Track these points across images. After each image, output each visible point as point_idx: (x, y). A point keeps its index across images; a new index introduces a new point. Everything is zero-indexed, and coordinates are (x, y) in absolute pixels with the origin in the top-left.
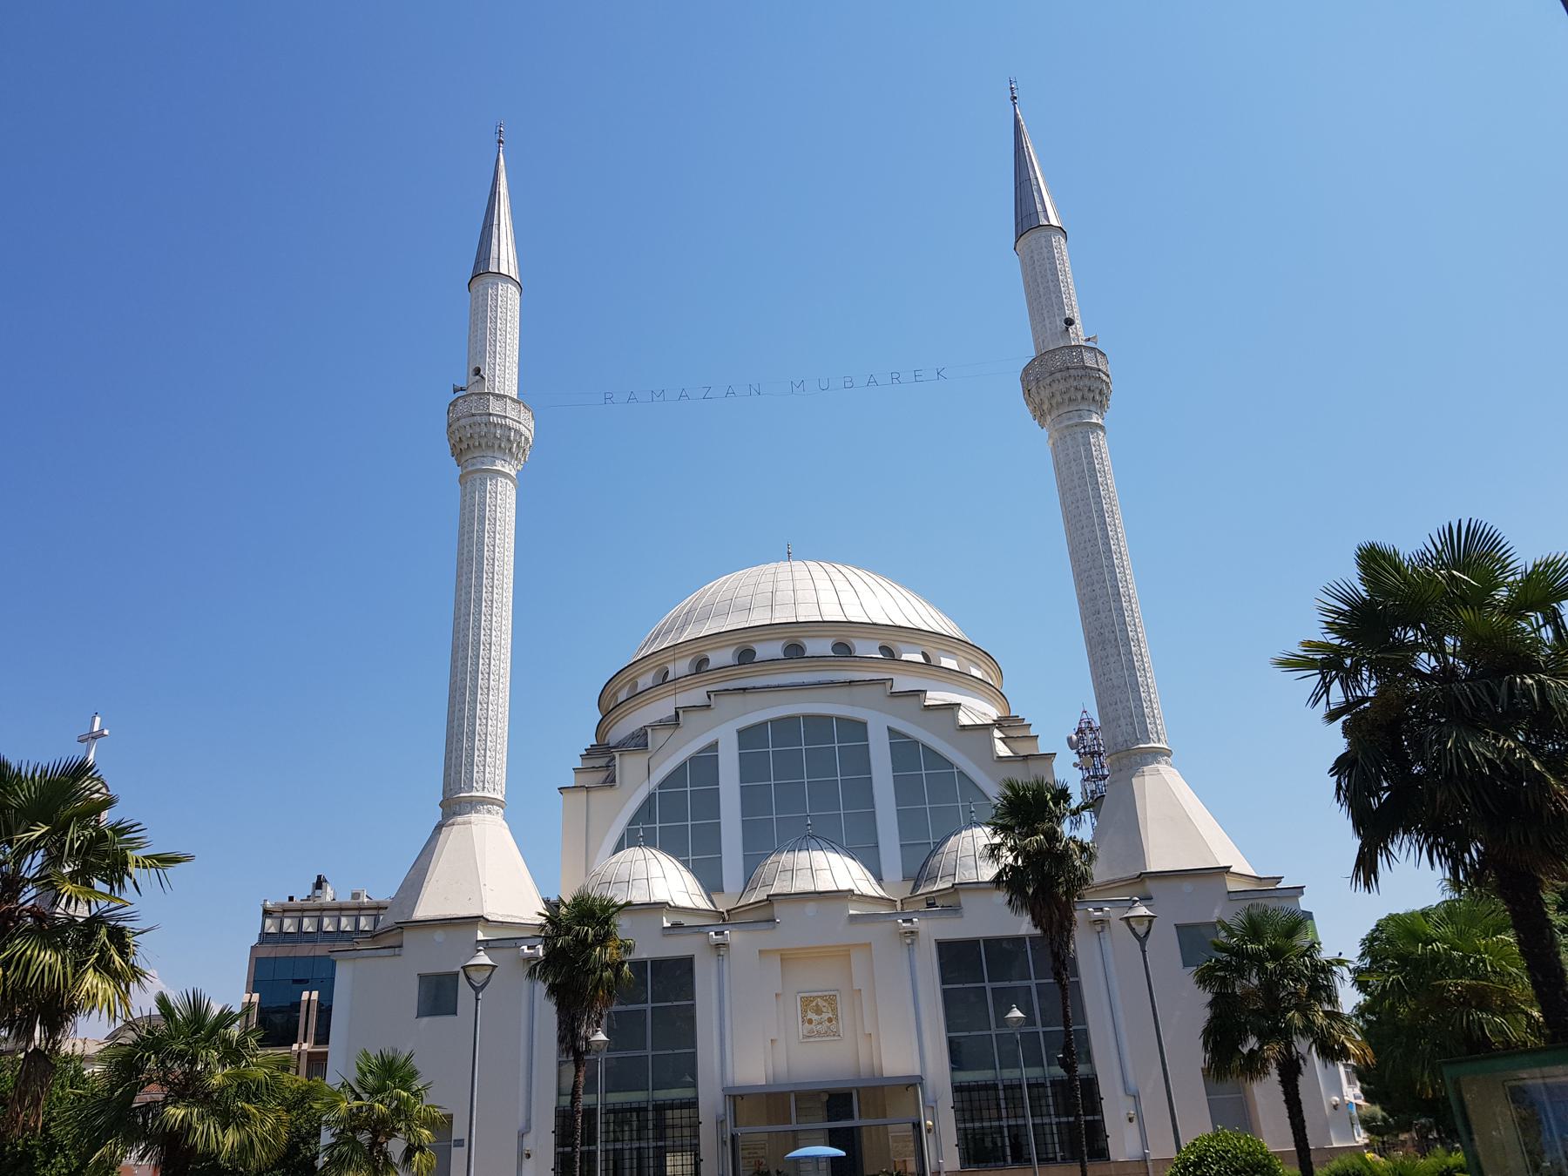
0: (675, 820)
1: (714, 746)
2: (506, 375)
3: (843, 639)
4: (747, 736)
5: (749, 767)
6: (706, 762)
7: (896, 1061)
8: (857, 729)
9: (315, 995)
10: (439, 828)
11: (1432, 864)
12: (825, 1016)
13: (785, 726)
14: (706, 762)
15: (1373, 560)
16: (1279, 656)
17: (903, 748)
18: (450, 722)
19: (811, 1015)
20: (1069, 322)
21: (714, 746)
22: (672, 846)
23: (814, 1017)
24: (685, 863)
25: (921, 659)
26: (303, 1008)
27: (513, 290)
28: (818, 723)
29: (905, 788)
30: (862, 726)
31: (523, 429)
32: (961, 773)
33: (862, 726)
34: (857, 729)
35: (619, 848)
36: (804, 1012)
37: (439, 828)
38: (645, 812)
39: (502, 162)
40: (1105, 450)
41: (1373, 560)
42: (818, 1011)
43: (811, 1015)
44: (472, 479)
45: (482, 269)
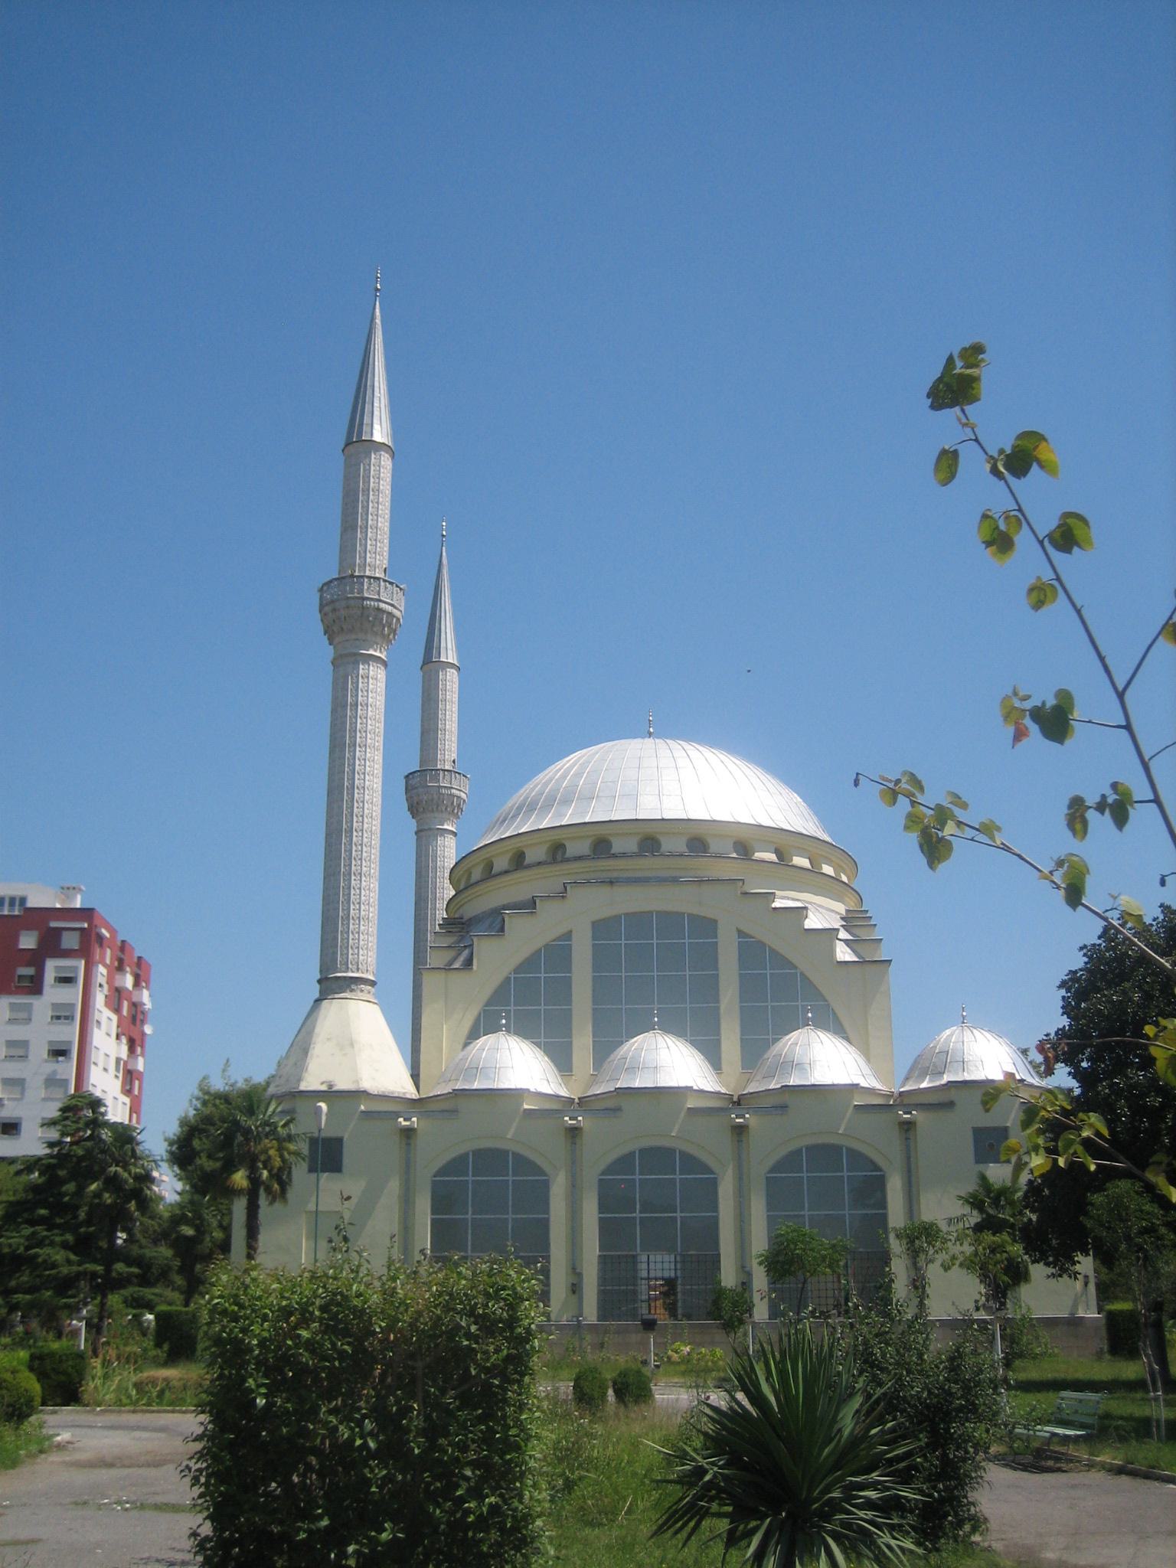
0: (528, 1003)
1: (568, 936)
2: (377, 553)
3: (697, 838)
4: (602, 928)
5: (602, 959)
8: (707, 927)
10: (318, 1001)
13: (638, 921)
14: (558, 953)
16: (1167, 903)
17: (752, 951)
18: (333, 725)
21: (568, 936)
22: (524, 1029)
24: (538, 1045)
25: (773, 857)
27: (386, 461)
28: (670, 921)
31: (395, 612)
34: (707, 927)
35: (474, 1035)
37: (318, 1001)
38: (499, 996)
39: (377, 310)
40: (1013, 1116)
44: (346, 663)
45: (357, 444)
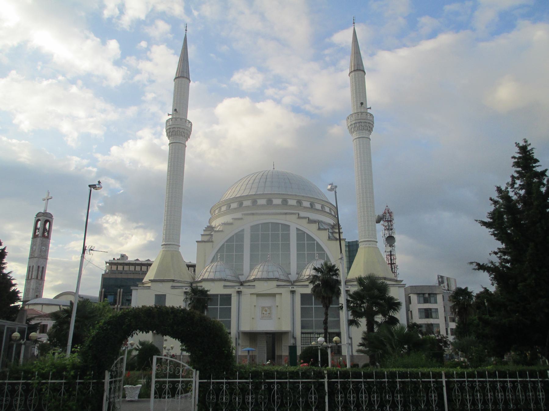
5: (253, 239)
7: (285, 327)
8: (288, 227)
9: (122, 290)
11: (538, 166)
12: (268, 312)
15: (466, 288)
19: (264, 312)
21: (243, 230)
23: (265, 313)
26: (118, 294)
28: (275, 225)
29: (300, 247)
30: (289, 226)
32: (317, 243)
33: (289, 226)
34: (287, 227)
36: (262, 311)
37: (349, 334)
41: (466, 288)
42: (266, 311)
43: (264, 312)
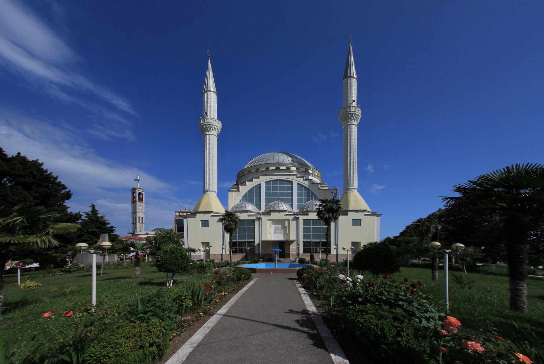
1: (260, 184)
5: (268, 189)
6: (259, 187)
14: (259, 187)
20: (354, 101)
